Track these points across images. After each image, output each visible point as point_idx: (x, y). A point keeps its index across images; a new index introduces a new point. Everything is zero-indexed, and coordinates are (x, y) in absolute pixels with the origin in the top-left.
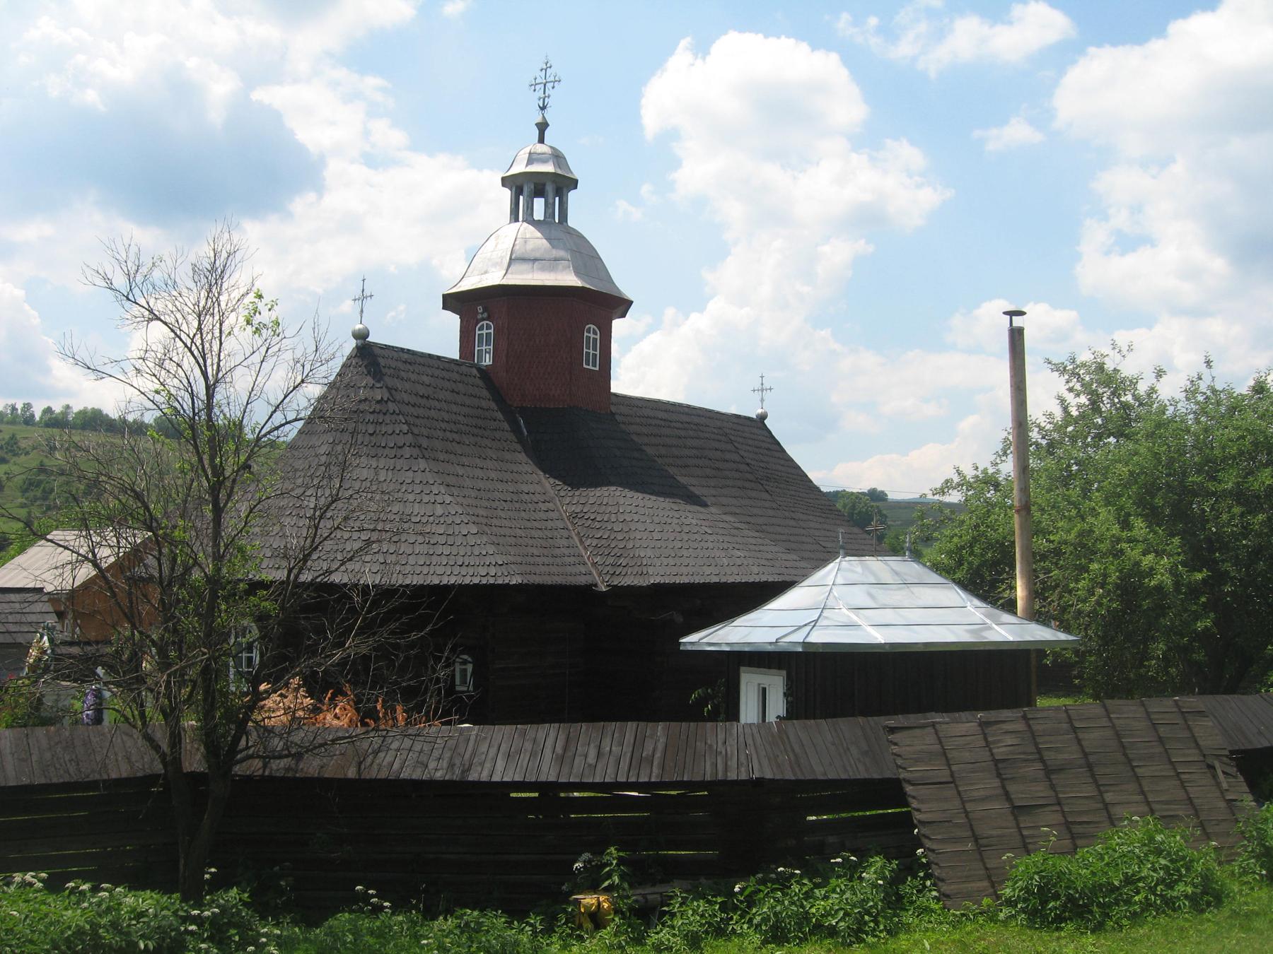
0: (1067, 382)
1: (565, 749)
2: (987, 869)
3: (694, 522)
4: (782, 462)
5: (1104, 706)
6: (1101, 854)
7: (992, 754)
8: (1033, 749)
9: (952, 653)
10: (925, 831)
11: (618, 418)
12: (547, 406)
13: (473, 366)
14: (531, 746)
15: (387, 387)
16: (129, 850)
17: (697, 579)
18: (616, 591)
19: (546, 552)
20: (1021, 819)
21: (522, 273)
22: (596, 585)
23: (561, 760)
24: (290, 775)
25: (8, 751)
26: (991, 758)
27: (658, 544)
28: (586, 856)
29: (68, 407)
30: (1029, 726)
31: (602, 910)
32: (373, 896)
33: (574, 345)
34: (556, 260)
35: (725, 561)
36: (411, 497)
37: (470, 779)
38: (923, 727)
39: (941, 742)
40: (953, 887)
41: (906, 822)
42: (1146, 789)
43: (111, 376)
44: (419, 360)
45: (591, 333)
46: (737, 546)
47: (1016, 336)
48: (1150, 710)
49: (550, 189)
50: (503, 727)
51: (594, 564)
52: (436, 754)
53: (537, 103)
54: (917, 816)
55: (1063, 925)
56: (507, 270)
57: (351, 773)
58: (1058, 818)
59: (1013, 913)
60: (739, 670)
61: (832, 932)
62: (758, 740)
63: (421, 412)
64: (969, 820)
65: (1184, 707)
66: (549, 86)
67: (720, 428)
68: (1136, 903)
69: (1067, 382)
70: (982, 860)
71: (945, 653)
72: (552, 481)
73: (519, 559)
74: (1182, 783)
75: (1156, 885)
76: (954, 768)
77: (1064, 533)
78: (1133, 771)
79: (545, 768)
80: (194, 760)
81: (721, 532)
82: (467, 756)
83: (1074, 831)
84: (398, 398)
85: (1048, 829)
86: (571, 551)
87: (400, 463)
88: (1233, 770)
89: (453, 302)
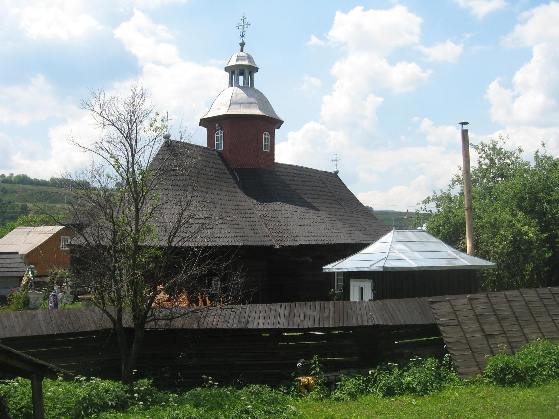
0: (479, 154)
1: (290, 313)
2: (477, 362)
4: (346, 192)
5: (520, 291)
6: (526, 354)
7: (475, 313)
8: (492, 310)
9: (443, 271)
10: (449, 346)
12: (248, 168)
13: (214, 150)
14: (274, 313)
16: (330, 290)
17: (319, 243)
18: (283, 248)
19: (252, 231)
22: (274, 246)
23: (288, 319)
24: (168, 328)
25: (42, 319)
26: (474, 314)
27: (301, 227)
28: (303, 360)
29: (12, 174)
30: (489, 300)
31: (310, 384)
32: (210, 380)
33: (259, 141)
35: (330, 234)
37: (249, 327)
38: (445, 301)
39: (453, 308)
40: (463, 370)
41: (441, 342)
42: (540, 327)
43: (90, 150)
45: (266, 135)
47: (465, 134)
48: (539, 293)
49: (246, 72)
50: (261, 305)
51: (273, 236)
52: (232, 317)
53: (239, 34)
54: (446, 340)
55: (514, 385)
56: (229, 108)
57: (195, 326)
58: (505, 340)
59: (491, 380)
60: (349, 280)
61: (414, 390)
62: (375, 308)
64: (467, 341)
65: (553, 292)
66: (245, 26)
68: (544, 375)
69: (479, 154)
70: (474, 358)
72: (252, 200)
73: (241, 235)
74: (555, 324)
75: (552, 367)
76: (459, 319)
77: (486, 218)
78: (534, 319)
79: (282, 322)
80: (128, 321)
81: (327, 222)
82: (246, 318)
83: (512, 345)
85: (502, 345)
86: (263, 231)
89: (204, 122)
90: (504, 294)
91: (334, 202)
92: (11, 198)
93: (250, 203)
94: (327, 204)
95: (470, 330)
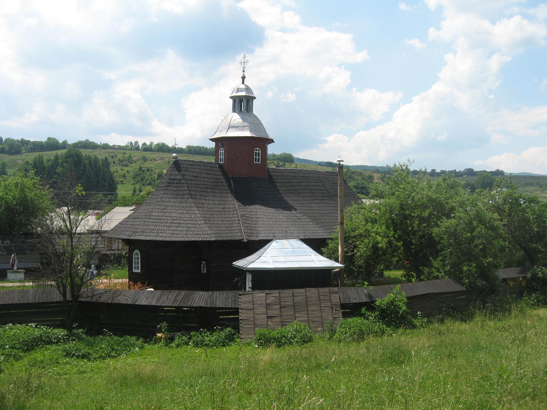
1: (160, 297)
3: (281, 217)
11: (273, 177)
15: (182, 175)
19: (227, 229)
20: (269, 320)
21: (232, 132)
22: (243, 240)
23: (158, 300)
24: (96, 301)
25: (31, 294)
29: (152, 143)
34: (244, 126)
36: (185, 212)
37: (136, 304)
41: (237, 320)
44: (196, 163)
45: (258, 150)
46: (293, 226)
49: (244, 100)
54: (240, 318)
57: (110, 302)
63: (193, 182)
66: (245, 63)
67: (318, 177)
71: (302, 270)
72: (238, 203)
73: (216, 232)
84: (185, 178)
86: (238, 228)
87: (183, 200)
88: (339, 309)
90: (293, 291)
91: (328, 198)
92: (150, 166)
93: (236, 205)
94: (318, 201)
95: (258, 312)
